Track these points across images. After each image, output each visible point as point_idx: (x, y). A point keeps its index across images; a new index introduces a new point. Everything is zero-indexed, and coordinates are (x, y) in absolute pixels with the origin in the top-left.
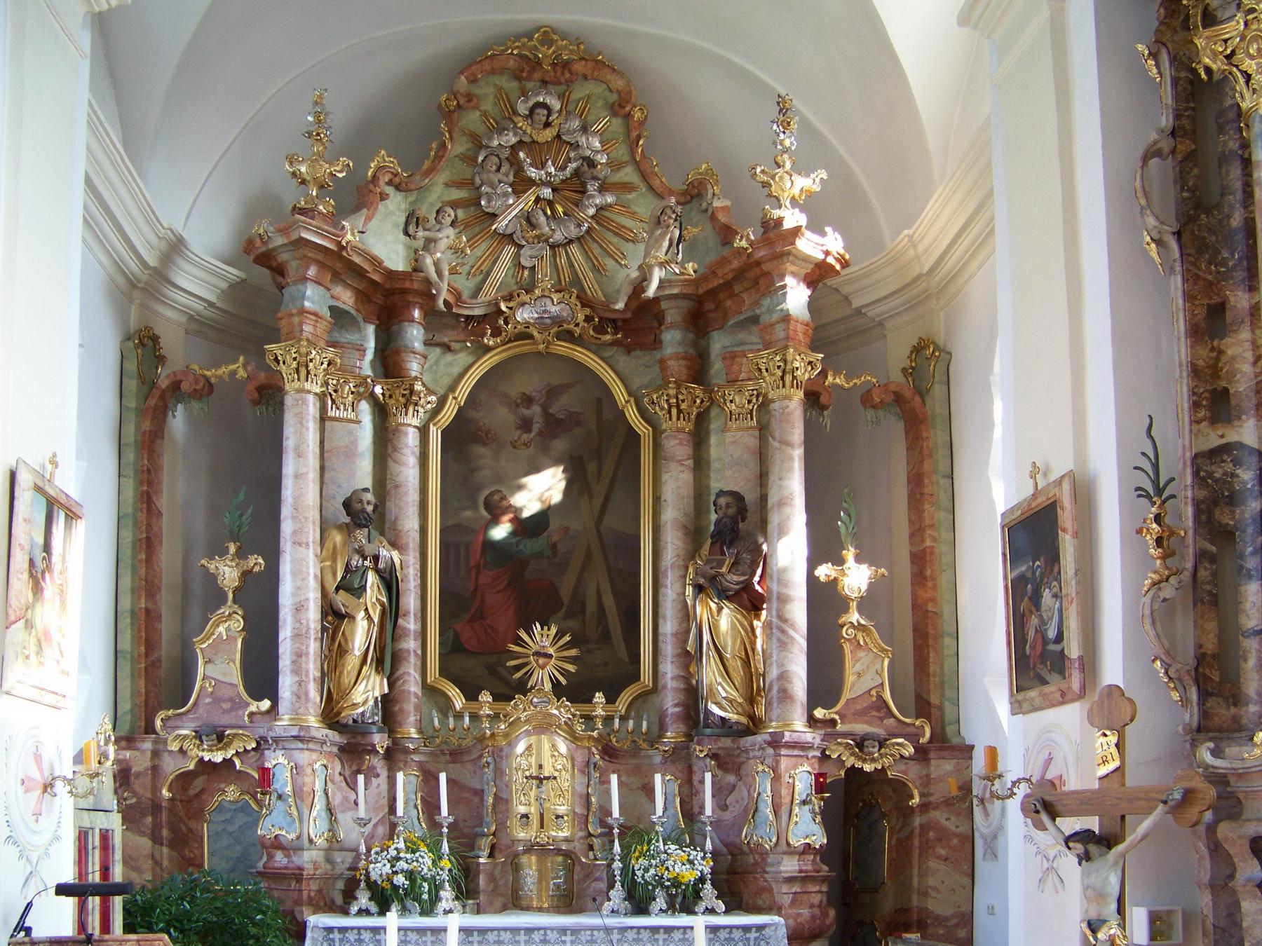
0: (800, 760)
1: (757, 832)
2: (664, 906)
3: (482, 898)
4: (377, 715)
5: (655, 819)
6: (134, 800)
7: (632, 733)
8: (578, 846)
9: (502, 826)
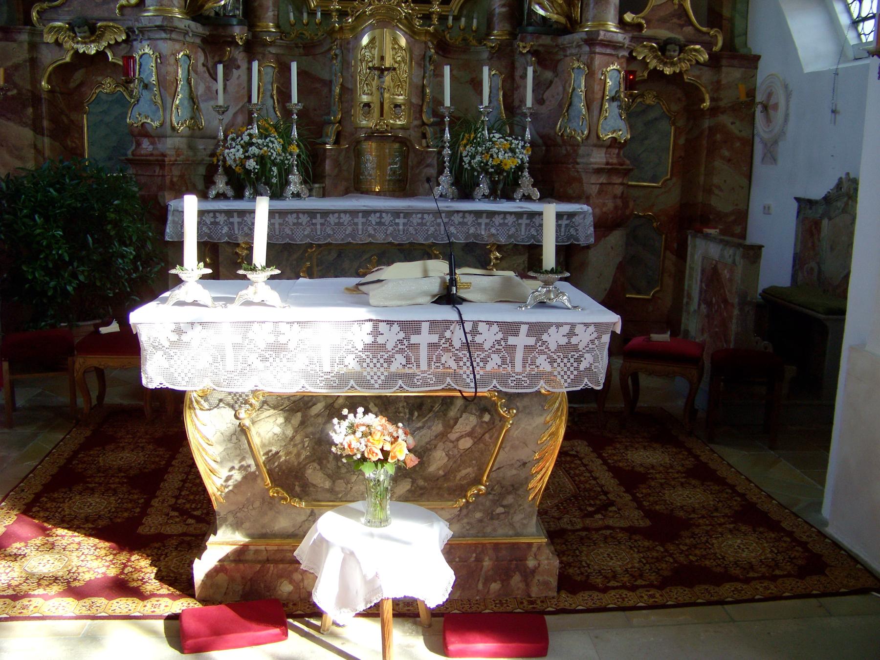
0: (611, 59)
1: (571, 125)
2: (487, 192)
3: (328, 181)
4: (238, 9)
5: (481, 108)
6: (15, 92)
7: (464, 29)
8: (413, 134)
9: (347, 114)
